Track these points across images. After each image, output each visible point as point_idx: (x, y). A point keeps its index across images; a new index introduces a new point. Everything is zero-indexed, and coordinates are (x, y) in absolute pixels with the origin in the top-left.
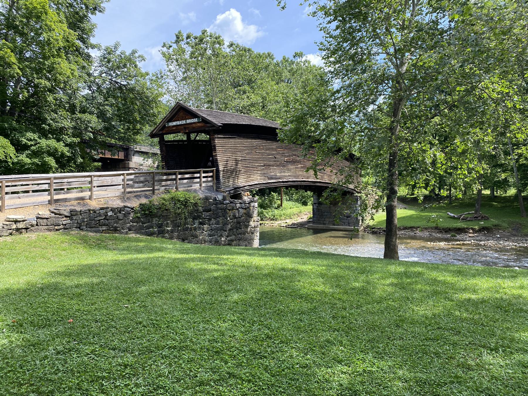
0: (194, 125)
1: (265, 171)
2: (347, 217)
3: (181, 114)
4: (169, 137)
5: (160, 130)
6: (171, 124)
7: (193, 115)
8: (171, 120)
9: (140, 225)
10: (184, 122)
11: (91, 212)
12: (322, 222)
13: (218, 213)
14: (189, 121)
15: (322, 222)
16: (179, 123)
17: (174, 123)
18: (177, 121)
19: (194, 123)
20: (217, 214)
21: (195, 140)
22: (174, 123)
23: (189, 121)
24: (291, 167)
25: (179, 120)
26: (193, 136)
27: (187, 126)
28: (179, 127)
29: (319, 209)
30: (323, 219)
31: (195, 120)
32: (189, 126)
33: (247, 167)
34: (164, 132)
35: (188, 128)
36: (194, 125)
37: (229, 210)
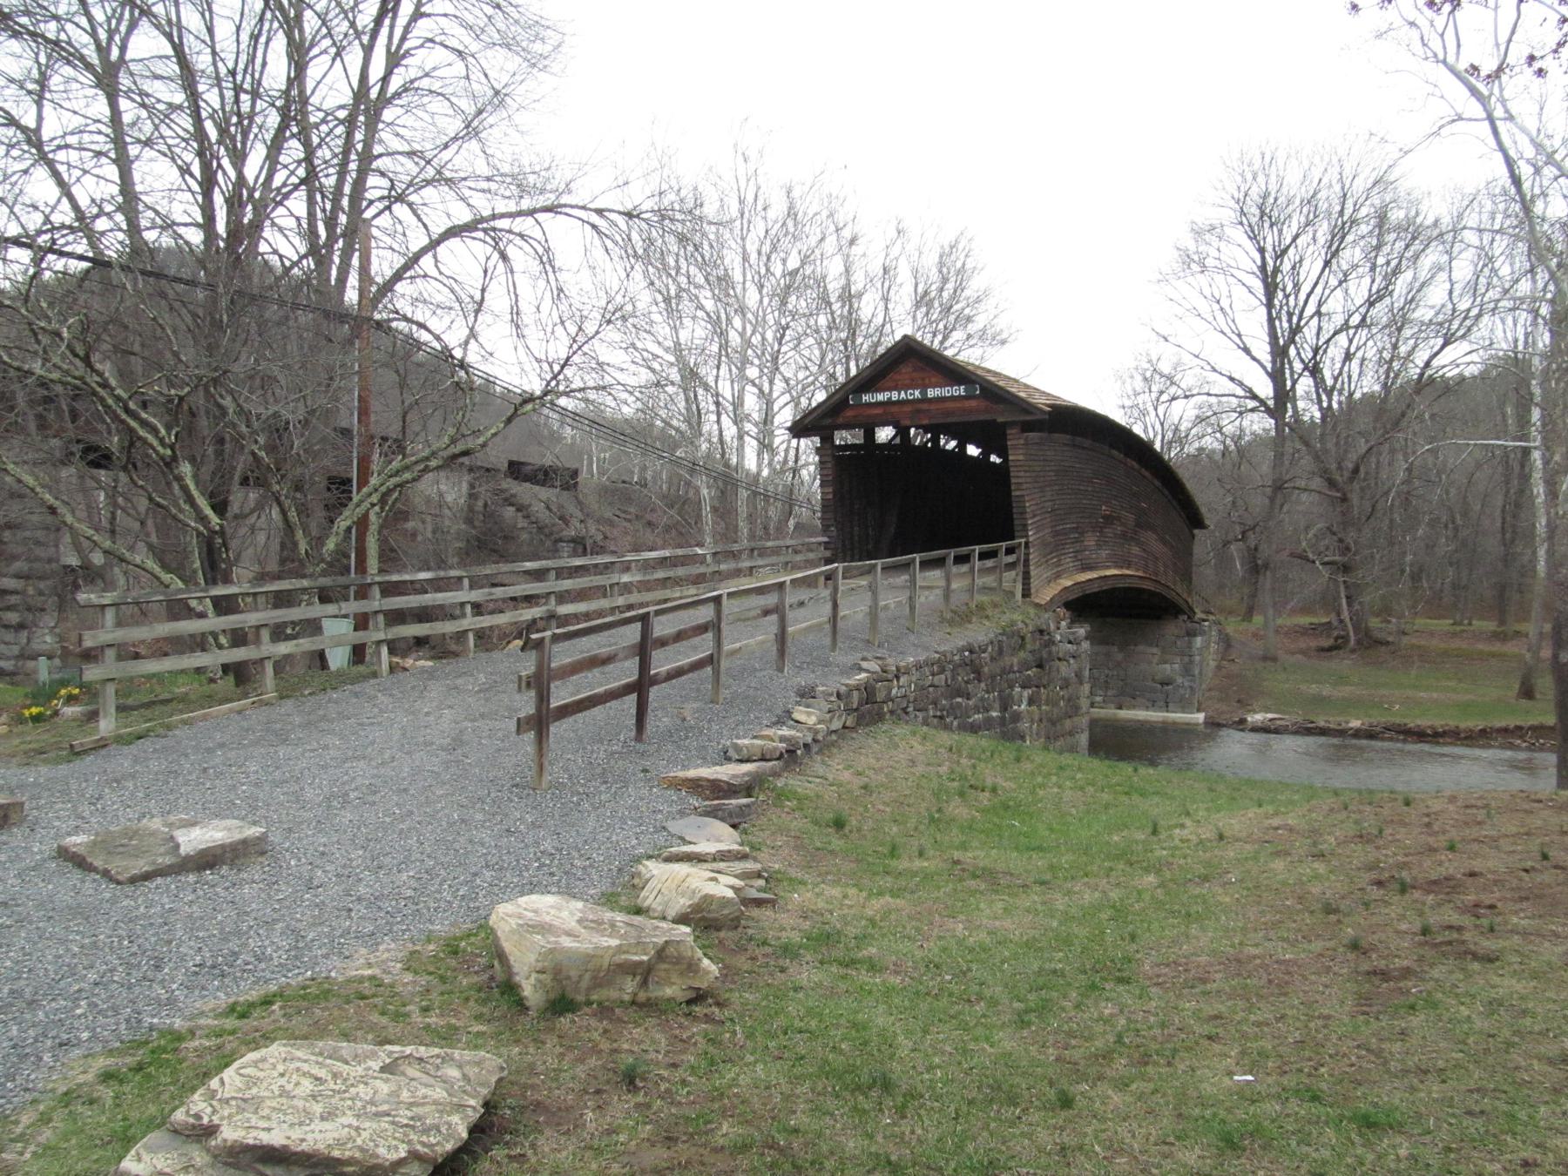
3: (906, 370)
6: (866, 398)
17: (880, 397)
18: (890, 389)
22: (880, 397)
23: (931, 393)
27: (925, 406)
28: (895, 409)
31: (960, 391)
32: (933, 407)
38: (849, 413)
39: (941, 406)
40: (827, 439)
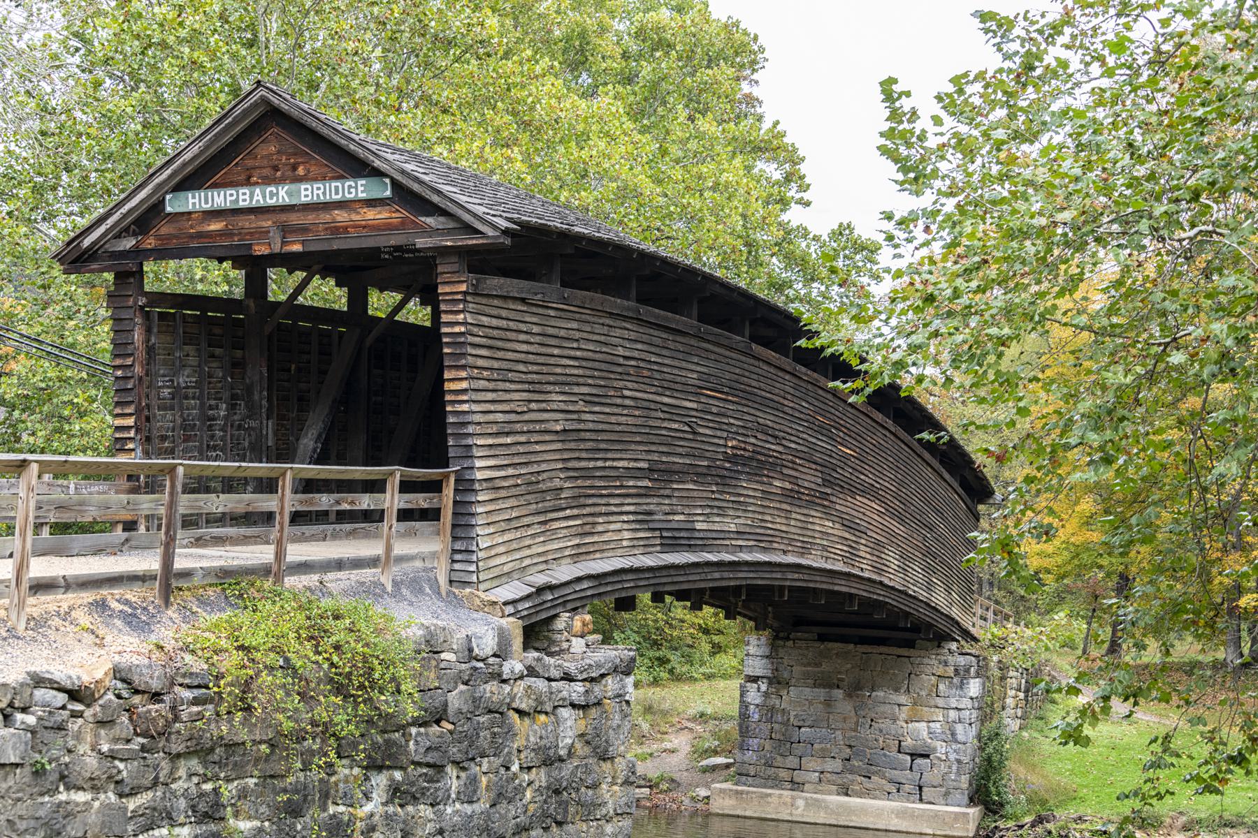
0: (341, 216)
1: (651, 504)
2: (914, 756)
3: (268, 147)
4: (165, 276)
5: (121, 232)
6: (195, 201)
7: (353, 164)
8: (195, 178)
9: (109, 806)
10: (281, 195)
11: (87, 748)
12: (783, 774)
13: (478, 729)
14: (309, 192)
15: (783, 774)
16: (245, 197)
17: (220, 199)
19: (342, 205)
20: (472, 739)
21: (291, 308)
22: (220, 199)
23: (309, 192)
24: (749, 487)
25: (248, 182)
26: (279, 286)
27: (294, 219)
29: (772, 709)
30: (792, 761)
31: (358, 189)
32: (310, 218)
33: (586, 474)
34: (150, 243)
35: (304, 230)
36: (341, 216)
37: (520, 713)
38: (165, 229)
39: (325, 217)
40: (128, 276)
